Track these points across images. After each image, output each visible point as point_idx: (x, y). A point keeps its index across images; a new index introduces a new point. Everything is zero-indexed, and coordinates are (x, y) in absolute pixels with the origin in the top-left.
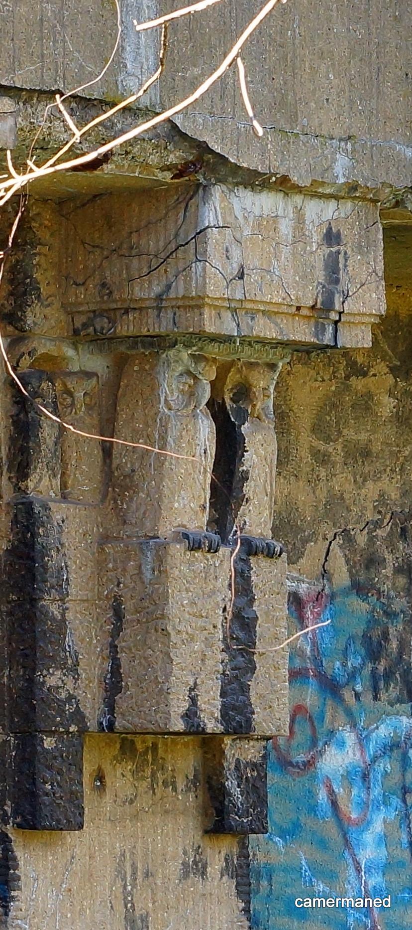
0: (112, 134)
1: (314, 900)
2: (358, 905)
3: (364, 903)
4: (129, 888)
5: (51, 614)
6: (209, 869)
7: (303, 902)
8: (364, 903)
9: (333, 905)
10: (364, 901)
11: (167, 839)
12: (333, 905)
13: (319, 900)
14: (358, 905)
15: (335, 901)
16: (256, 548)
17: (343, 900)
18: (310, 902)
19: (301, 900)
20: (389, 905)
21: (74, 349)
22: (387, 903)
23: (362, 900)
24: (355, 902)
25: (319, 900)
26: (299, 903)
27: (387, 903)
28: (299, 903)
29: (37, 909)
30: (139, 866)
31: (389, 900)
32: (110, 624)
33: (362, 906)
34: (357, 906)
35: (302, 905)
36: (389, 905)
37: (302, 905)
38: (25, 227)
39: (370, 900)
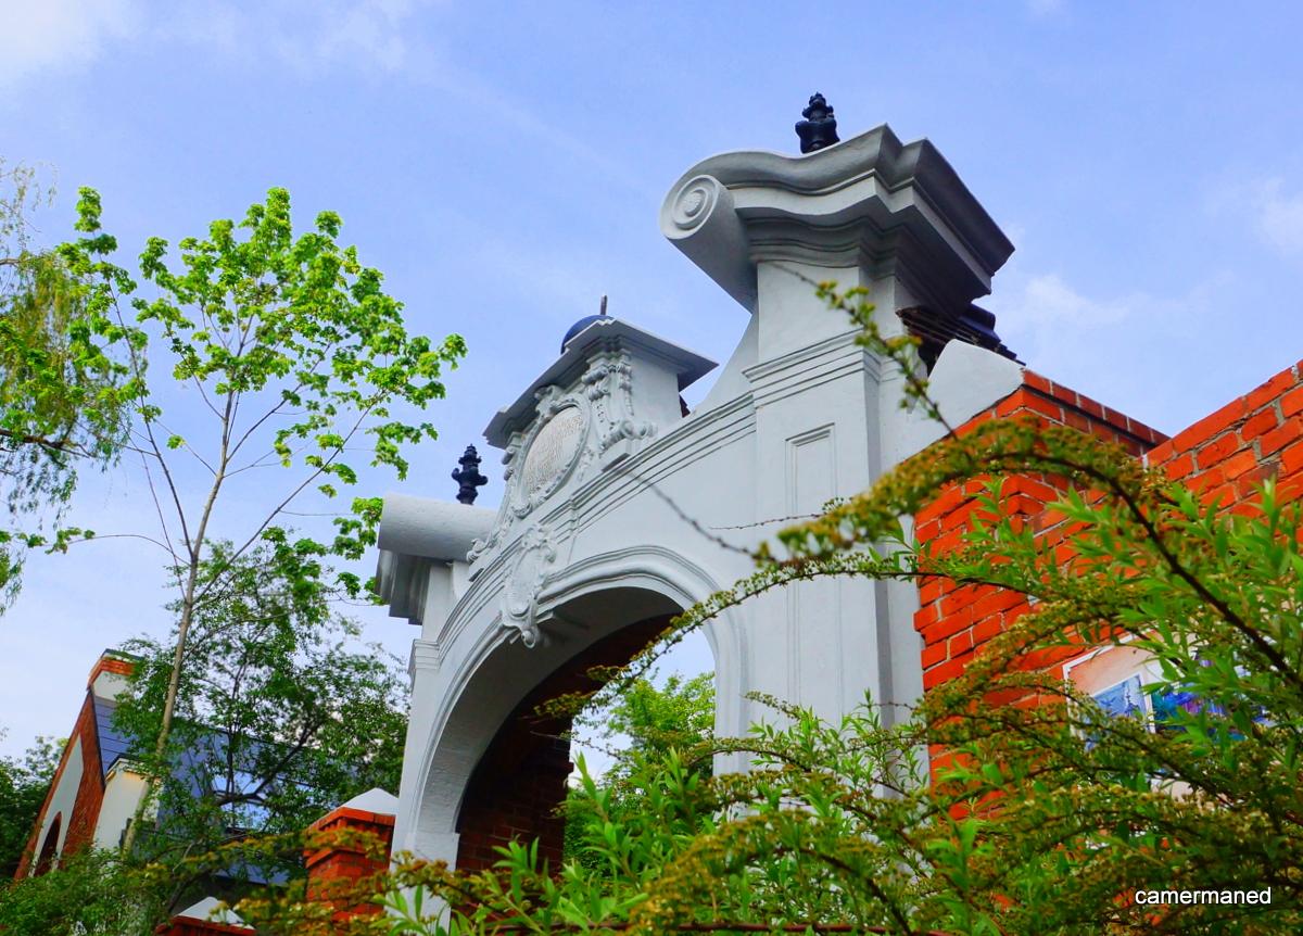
0: (276, 232)
1: (1236, 893)
2: (1225, 900)
5: (283, 575)
6: (94, 905)
7: (1147, 897)
11: (1000, 756)
13: (1170, 894)
14: (1225, 900)
16: (410, 581)
17: (1204, 893)
18: (1230, 897)
20: (1269, 901)
22: (1265, 897)
24: (1220, 896)
25: (1170, 894)
26: (1141, 897)
27: (1265, 897)
28: (1141, 897)
31: (1269, 893)
35: (1145, 901)
37: (1145, 901)
38: (67, 397)
39: (1216, 893)
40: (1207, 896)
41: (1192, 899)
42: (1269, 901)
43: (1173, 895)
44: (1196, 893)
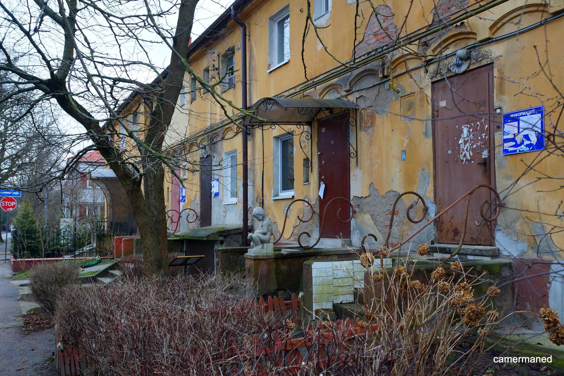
1: (537, 358)
7: (498, 360)
13: (526, 358)
17: (523, 358)
18: (534, 360)
20: (551, 362)
22: (549, 360)
25: (526, 358)
26: (496, 360)
28: (496, 360)
31: (551, 358)
39: (528, 358)
40: (524, 359)
42: (551, 362)
44: (519, 358)
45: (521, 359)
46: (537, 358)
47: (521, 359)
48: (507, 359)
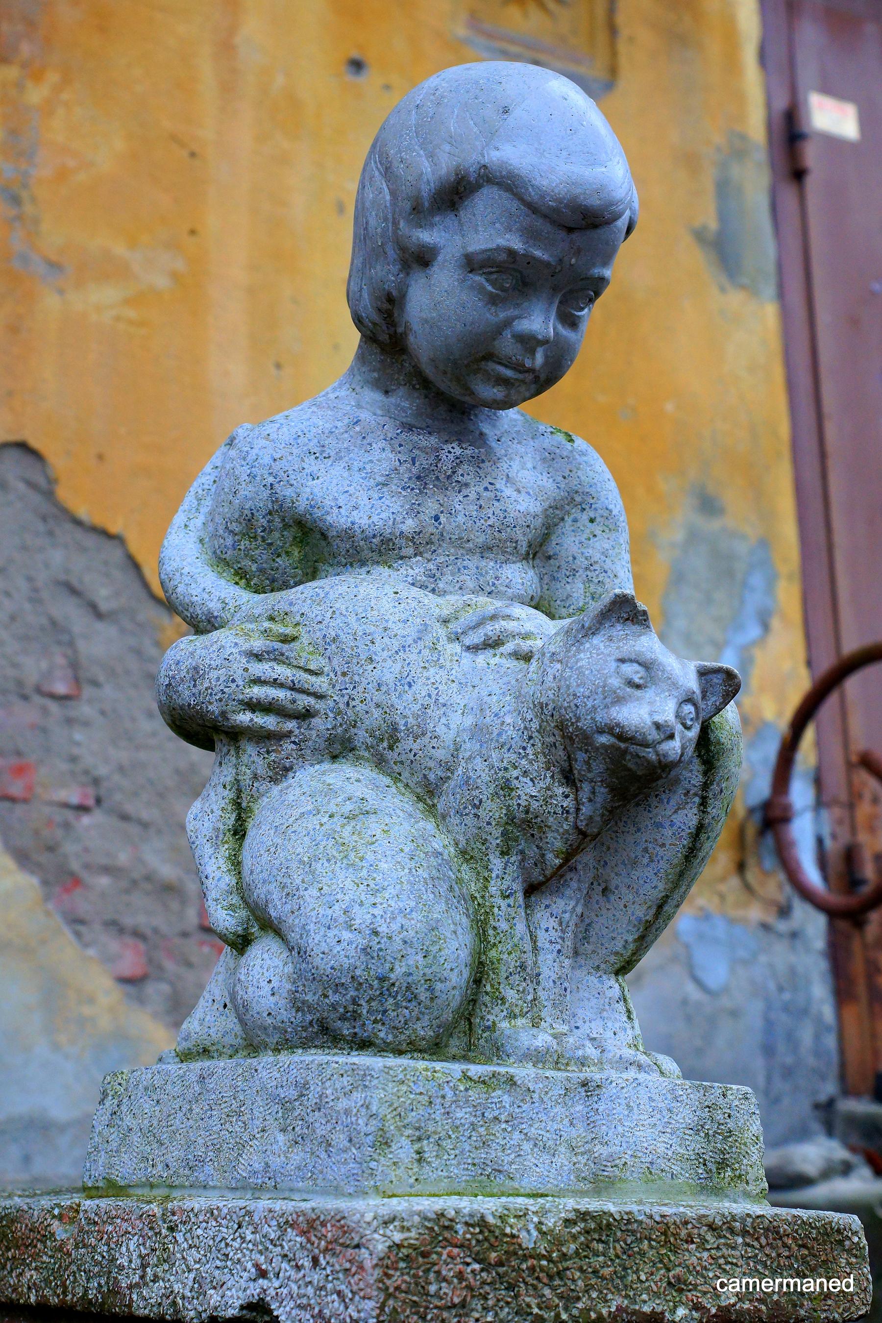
1: (744, 1281)
2: (807, 1288)
3: (815, 1285)
4: (690, 1287)
8: (815, 1285)
9: (771, 1289)
10: (741, 1282)
12: (771, 1289)
13: (751, 1281)
15: (774, 1283)
17: (785, 1281)
19: (726, 1282)
21: (556, 210)
22: (848, 1287)
23: (737, 1280)
25: (751, 1281)
29: (304, 1301)
30: (124, 1203)
31: (851, 1281)
32: (702, 715)
33: (738, 1289)
34: (805, 1290)
36: (851, 1289)
39: (798, 1280)
41: (774, 1287)
43: (755, 1282)
45: (781, 1285)
46: (818, 1281)
47: (781, 1285)
48: (748, 1283)
